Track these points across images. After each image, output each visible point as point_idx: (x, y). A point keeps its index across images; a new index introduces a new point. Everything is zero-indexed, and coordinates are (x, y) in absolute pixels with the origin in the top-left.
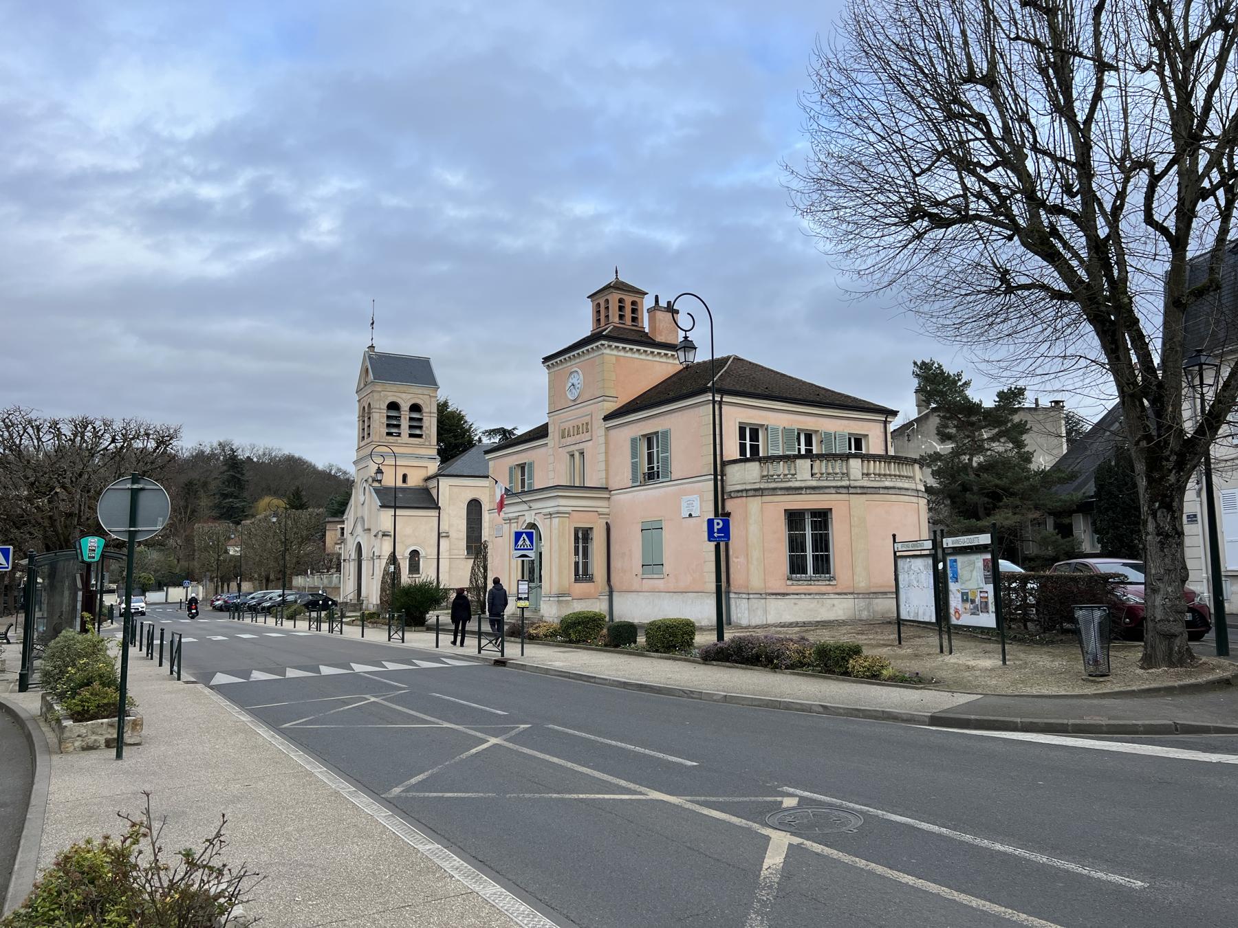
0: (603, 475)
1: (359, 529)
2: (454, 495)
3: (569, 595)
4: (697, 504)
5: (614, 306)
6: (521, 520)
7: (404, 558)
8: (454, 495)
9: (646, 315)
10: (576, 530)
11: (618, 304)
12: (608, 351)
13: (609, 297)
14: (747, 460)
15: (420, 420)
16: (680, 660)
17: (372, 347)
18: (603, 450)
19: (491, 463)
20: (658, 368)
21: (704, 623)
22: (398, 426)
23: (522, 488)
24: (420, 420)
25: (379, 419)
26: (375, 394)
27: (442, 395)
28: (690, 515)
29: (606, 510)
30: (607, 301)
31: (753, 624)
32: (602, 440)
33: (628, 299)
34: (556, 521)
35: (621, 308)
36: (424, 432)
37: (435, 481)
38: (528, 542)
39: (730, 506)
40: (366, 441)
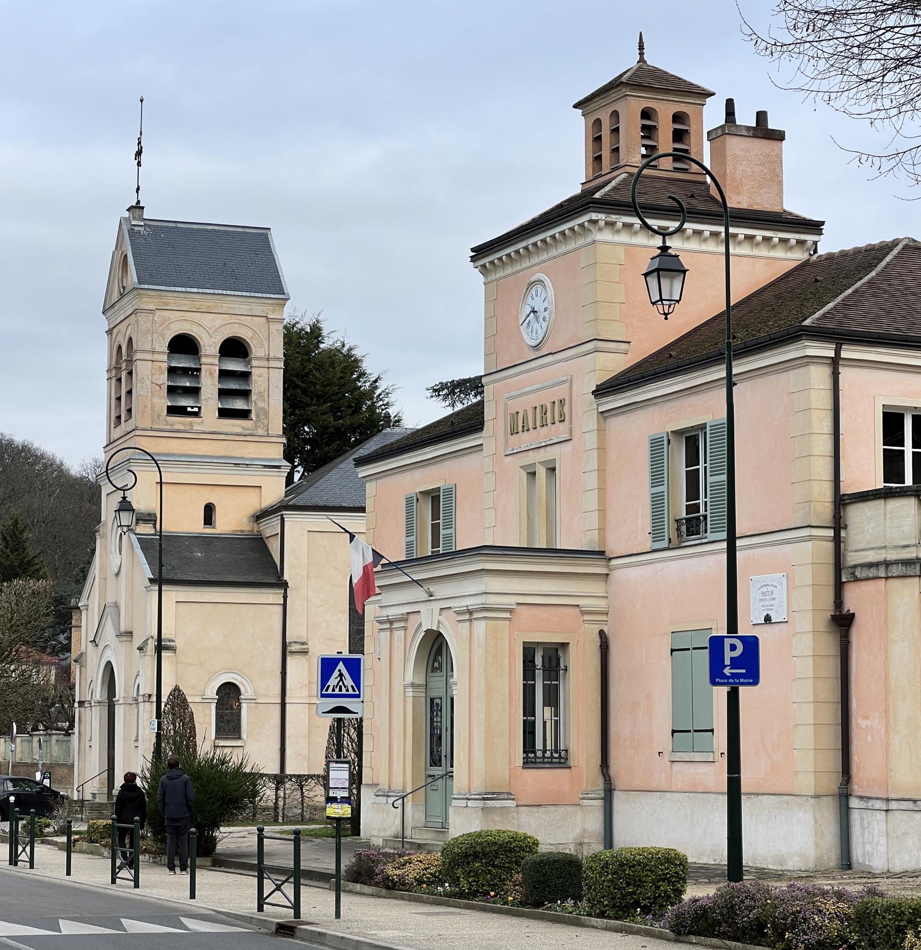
0: (593, 521)
1: (109, 632)
2: (320, 555)
3: (509, 796)
4: (781, 593)
5: (631, 127)
6: (413, 621)
7: (205, 701)
8: (320, 555)
9: (707, 145)
10: (529, 651)
11: (639, 122)
12: (606, 236)
13: (620, 107)
14: (903, 493)
15: (246, 376)
16: (638, 932)
17: (137, 208)
18: (594, 464)
19: (370, 487)
20: (721, 272)
21: (706, 860)
22: (194, 392)
23: (435, 548)
24: (246, 376)
25: (152, 374)
26: (142, 318)
27: (299, 311)
28: (768, 619)
29: (601, 604)
30: (615, 115)
31: (897, 868)
32: (591, 440)
33: (665, 109)
34: (480, 627)
35: (649, 131)
36: (255, 404)
37: (276, 521)
38: (349, 682)
39: (857, 598)
40: (124, 427)
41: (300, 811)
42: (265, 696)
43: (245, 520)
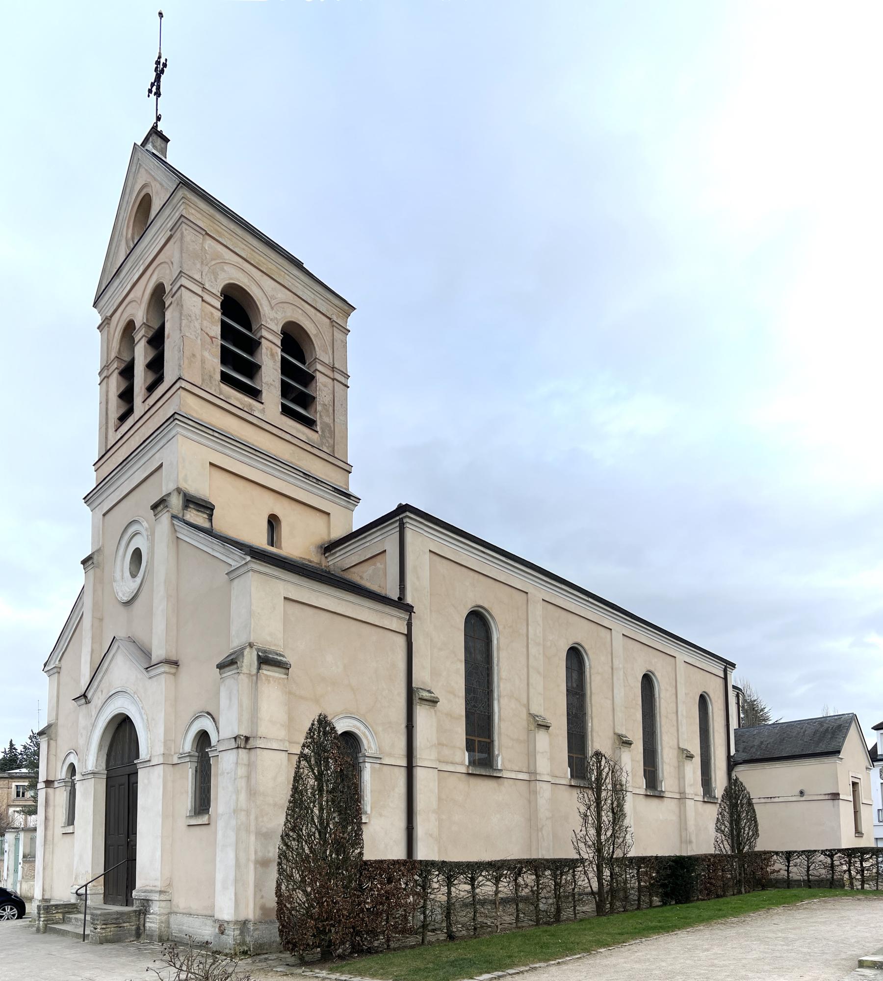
41: (578, 908)
42: (390, 755)
43: (313, 549)
